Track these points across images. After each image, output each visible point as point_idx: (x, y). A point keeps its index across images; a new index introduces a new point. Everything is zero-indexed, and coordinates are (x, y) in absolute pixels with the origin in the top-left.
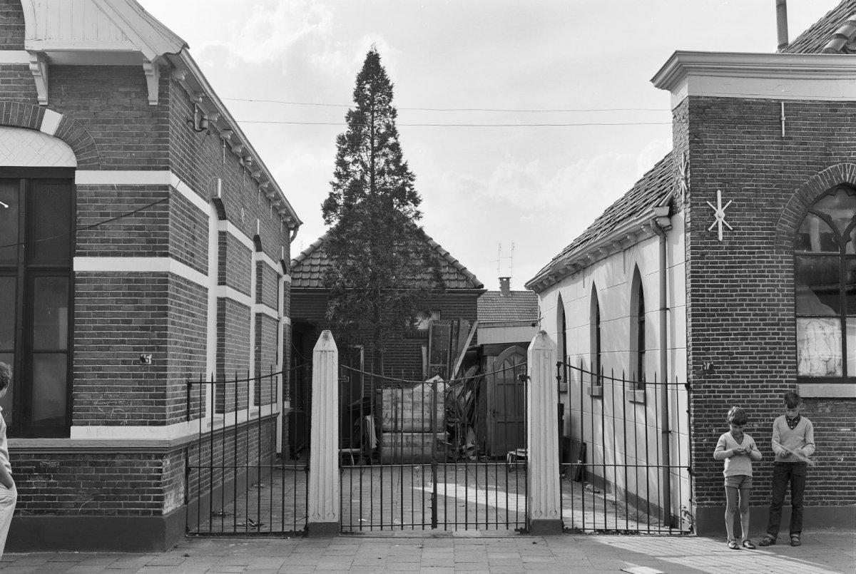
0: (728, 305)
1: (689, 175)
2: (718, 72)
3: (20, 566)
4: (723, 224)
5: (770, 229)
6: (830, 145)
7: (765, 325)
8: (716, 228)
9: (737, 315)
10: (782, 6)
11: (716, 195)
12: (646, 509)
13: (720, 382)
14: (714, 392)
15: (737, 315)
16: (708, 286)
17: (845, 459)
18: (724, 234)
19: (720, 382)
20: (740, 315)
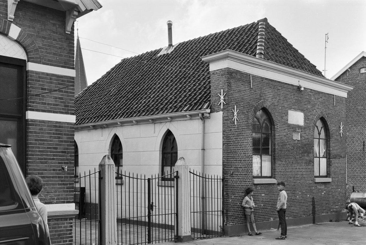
8: (234, 120)
11: (234, 108)
17: (263, 205)
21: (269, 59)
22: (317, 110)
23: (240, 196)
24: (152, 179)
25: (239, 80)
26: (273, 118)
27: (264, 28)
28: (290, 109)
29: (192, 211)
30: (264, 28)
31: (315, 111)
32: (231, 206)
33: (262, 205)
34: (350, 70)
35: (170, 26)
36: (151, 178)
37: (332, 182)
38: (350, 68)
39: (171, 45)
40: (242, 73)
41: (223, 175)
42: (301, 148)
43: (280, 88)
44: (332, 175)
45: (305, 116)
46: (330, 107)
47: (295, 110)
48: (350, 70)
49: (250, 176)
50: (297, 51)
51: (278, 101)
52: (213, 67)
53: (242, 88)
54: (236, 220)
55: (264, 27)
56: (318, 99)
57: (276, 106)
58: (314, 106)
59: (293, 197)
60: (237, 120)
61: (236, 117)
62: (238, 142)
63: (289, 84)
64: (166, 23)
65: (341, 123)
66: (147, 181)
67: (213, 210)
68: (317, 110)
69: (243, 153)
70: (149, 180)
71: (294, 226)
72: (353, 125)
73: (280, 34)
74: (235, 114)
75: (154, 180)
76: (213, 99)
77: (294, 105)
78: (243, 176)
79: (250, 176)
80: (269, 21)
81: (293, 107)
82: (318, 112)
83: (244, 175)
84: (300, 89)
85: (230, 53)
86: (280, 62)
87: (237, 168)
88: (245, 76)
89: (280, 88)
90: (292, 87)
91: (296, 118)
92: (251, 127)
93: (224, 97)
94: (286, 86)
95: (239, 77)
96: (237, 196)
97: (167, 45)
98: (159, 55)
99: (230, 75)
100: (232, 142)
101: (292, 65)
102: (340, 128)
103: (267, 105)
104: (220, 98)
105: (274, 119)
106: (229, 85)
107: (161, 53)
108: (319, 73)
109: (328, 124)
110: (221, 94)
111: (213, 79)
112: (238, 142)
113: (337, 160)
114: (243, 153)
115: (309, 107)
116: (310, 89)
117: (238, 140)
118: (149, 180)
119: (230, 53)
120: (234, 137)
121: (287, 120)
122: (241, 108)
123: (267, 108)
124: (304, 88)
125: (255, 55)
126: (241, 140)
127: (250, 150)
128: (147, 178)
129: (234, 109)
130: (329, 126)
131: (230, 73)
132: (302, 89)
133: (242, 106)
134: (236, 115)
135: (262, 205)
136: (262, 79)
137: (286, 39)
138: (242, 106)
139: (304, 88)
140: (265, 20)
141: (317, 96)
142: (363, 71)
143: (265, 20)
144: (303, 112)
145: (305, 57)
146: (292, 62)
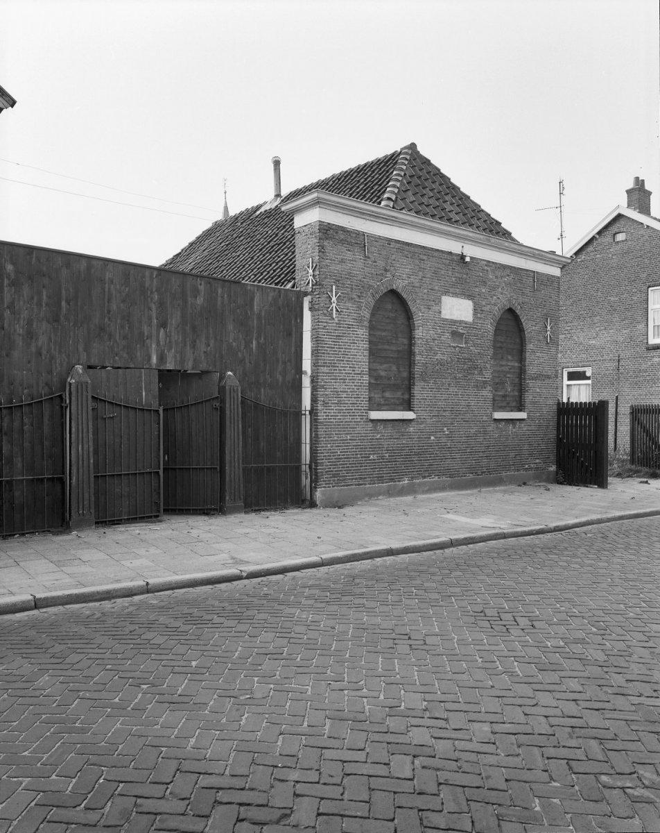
0: (337, 360)
1: (317, 273)
2: (338, 203)
3: (350, 244)
4: (336, 308)
5: (358, 314)
6: (318, 360)
7: (355, 374)
8: (332, 310)
9: (341, 367)
10: (659, 220)
11: (332, 289)
12: (186, 693)
13: (331, 410)
14: (328, 416)
15: (341, 367)
16: (327, 347)
17: (389, 456)
18: (336, 314)
19: (331, 410)
20: (343, 367)
21: (403, 208)
22: (500, 296)
23: (341, 440)
25: (342, 242)
26: (411, 308)
27: (406, 159)
28: (446, 293)
30: (406, 159)
31: (495, 297)
32: (325, 456)
33: (387, 455)
34: (598, 237)
35: (277, 163)
37: (528, 418)
38: (599, 233)
39: (278, 195)
40: (348, 231)
41: (312, 404)
42: (467, 361)
43: (425, 258)
44: (528, 405)
45: (475, 307)
46: (527, 291)
47: (455, 295)
48: (598, 237)
49: (363, 407)
50: (469, 197)
51: (421, 280)
52: (300, 221)
53: (349, 255)
54: (334, 481)
55: (408, 157)
56: (502, 277)
57: (417, 287)
58: (494, 288)
59: (449, 444)
60: (337, 310)
61: (334, 305)
62: (339, 348)
63: (442, 251)
64: (271, 158)
65: (547, 319)
68: (500, 296)
69: (350, 367)
71: (467, 490)
72: (602, 328)
73: (439, 170)
74: (334, 299)
76: (298, 275)
77: (453, 286)
78: (349, 406)
79: (363, 407)
80: (419, 149)
81: (451, 290)
82: (502, 299)
83: (351, 404)
84: (464, 260)
85: (322, 196)
86: (426, 214)
87: (337, 392)
88: (354, 235)
89: (425, 258)
90: (449, 257)
91: (458, 309)
92: (366, 323)
93: (313, 271)
94: (436, 254)
95: (342, 237)
96: (337, 440)
97: (272, 196)
98: (258, 213)
99: (323, 233)
100: (327, 347)
101: (449, 220)
102: (547, 327)
103: (399, 285)
104: (308, 272)
105: (413, 309)
106: (322, 250)
107: (267, 207)
108: (506, 234)
109: (522, 320)
110: (308, 267)
111: (299, 240)
112: (339, 348)
113: (539, 383)
114: (350, 367)
115: (484, 291)
116: (486, 261)
117: (339, 345)
119: (322, 196)
120: (331, 338)
121: (440, 312)
122: (345, 290)
123: (399, 291)
124: (471, 258)
125: (380, 203)
126: (345, 345)
127: (364, 362)
129: (332, 291)
130: (524, 324)
131: (326, 231)
132: (468, 259)
133: (347, 287)
134: (336, 302)
135: (387, 455)
136: (390, 241)
137: (448, 178)
138: (347, 287)
139: (471, 258)
140: (413, 146)
141: (499, 273)
142: (620, 237)
143: (413, 146)
144: (471, 299)
145: (483, 207)
146: (452, 215)
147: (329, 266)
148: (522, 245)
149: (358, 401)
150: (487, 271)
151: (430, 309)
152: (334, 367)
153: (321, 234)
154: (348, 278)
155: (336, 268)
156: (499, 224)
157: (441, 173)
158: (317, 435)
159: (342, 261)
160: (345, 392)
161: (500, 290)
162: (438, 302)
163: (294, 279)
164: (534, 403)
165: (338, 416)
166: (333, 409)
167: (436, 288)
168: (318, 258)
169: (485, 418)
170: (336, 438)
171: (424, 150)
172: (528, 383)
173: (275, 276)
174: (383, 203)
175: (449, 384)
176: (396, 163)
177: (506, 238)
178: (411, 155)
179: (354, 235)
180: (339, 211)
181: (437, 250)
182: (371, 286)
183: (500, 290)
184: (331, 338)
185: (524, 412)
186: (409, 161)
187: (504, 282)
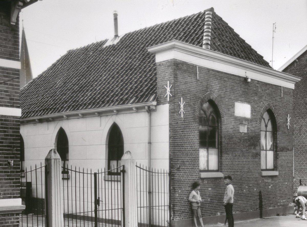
8: (181, 113)
17: (210, 200)
24: (98, 173)
25: (185, 71)
27: (210, 18)
28: (237, 100)
29: (139, 206)
30: (210, 18)
31: (262, 103)
36: (97, 173)
37: (279, 175)
39: (116, 36)
47: (242, 101)
49: (197, 170)
51: (225, 93)
52: (159, 58)
53: (189, 79)
55: (211, 16)
58: (261, 97)
62: (185, 135)
65: (288, 115)
66: (93, 176)
67: (160, 205)
70: (95, 174)
73: (227, 24)
75: (100, 175)
77: (240, 96)
78: (190, 170)
83: (191, 168)
87: (184, 161)
89: (226, 79)
91: (243, 110)
95: (185, 68)
96: (184, 191)
100: (179, 135)
102: (287, 120)
103: (214, 96)
106: (176, 77)
107: (107, 44)
108: (266, 64)
109: (275, 116)
111: (160, 70)
115: (256, 99)
118: (95, 174)
124: (251, 80)
128: (93, 172)
131: (177, 66)
132: (249, 80)
133: (188, 98)
135: (209, 199)
136: (209, 70)
139: (251, 80)
143: (212, 10)
147: (179, 86)
148: (275, 71)
149: (194, 167)
150: (258, 86)
151: (229, 110)
152: (182, 146)
153: (175, 67)
154: (188, 93)
155: (183, 87)
156: (262, 57)
157: (229, 26)
158: (174, 188)
159: (186, 83)
160: (188, 161)
161: (264, 98)
162: (233, 106)
163: (156, 93)
164: (282, 166)
165: (184, 176)
166: (182, 172)
167: (233, 98)
168: (173, 81)
169: (257, 176)
170: (183, 190)
171: (218, 12)
172: (279, 154)
173: (56, 95)
174: (204, 47)
175: (239, 155)
176: (204, 20)
177: (254, 63)
178: (212, 15)
179: (191, 67)
180: (209, 59)
181: (233, 75)
182: (200, 97)
183: (264, 98)
184: (181, 130)
185: (277, 171)
186: (212, 19)
187: (266, 93)
